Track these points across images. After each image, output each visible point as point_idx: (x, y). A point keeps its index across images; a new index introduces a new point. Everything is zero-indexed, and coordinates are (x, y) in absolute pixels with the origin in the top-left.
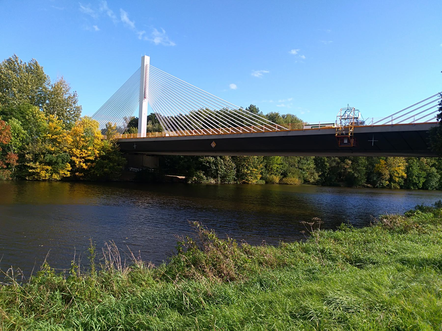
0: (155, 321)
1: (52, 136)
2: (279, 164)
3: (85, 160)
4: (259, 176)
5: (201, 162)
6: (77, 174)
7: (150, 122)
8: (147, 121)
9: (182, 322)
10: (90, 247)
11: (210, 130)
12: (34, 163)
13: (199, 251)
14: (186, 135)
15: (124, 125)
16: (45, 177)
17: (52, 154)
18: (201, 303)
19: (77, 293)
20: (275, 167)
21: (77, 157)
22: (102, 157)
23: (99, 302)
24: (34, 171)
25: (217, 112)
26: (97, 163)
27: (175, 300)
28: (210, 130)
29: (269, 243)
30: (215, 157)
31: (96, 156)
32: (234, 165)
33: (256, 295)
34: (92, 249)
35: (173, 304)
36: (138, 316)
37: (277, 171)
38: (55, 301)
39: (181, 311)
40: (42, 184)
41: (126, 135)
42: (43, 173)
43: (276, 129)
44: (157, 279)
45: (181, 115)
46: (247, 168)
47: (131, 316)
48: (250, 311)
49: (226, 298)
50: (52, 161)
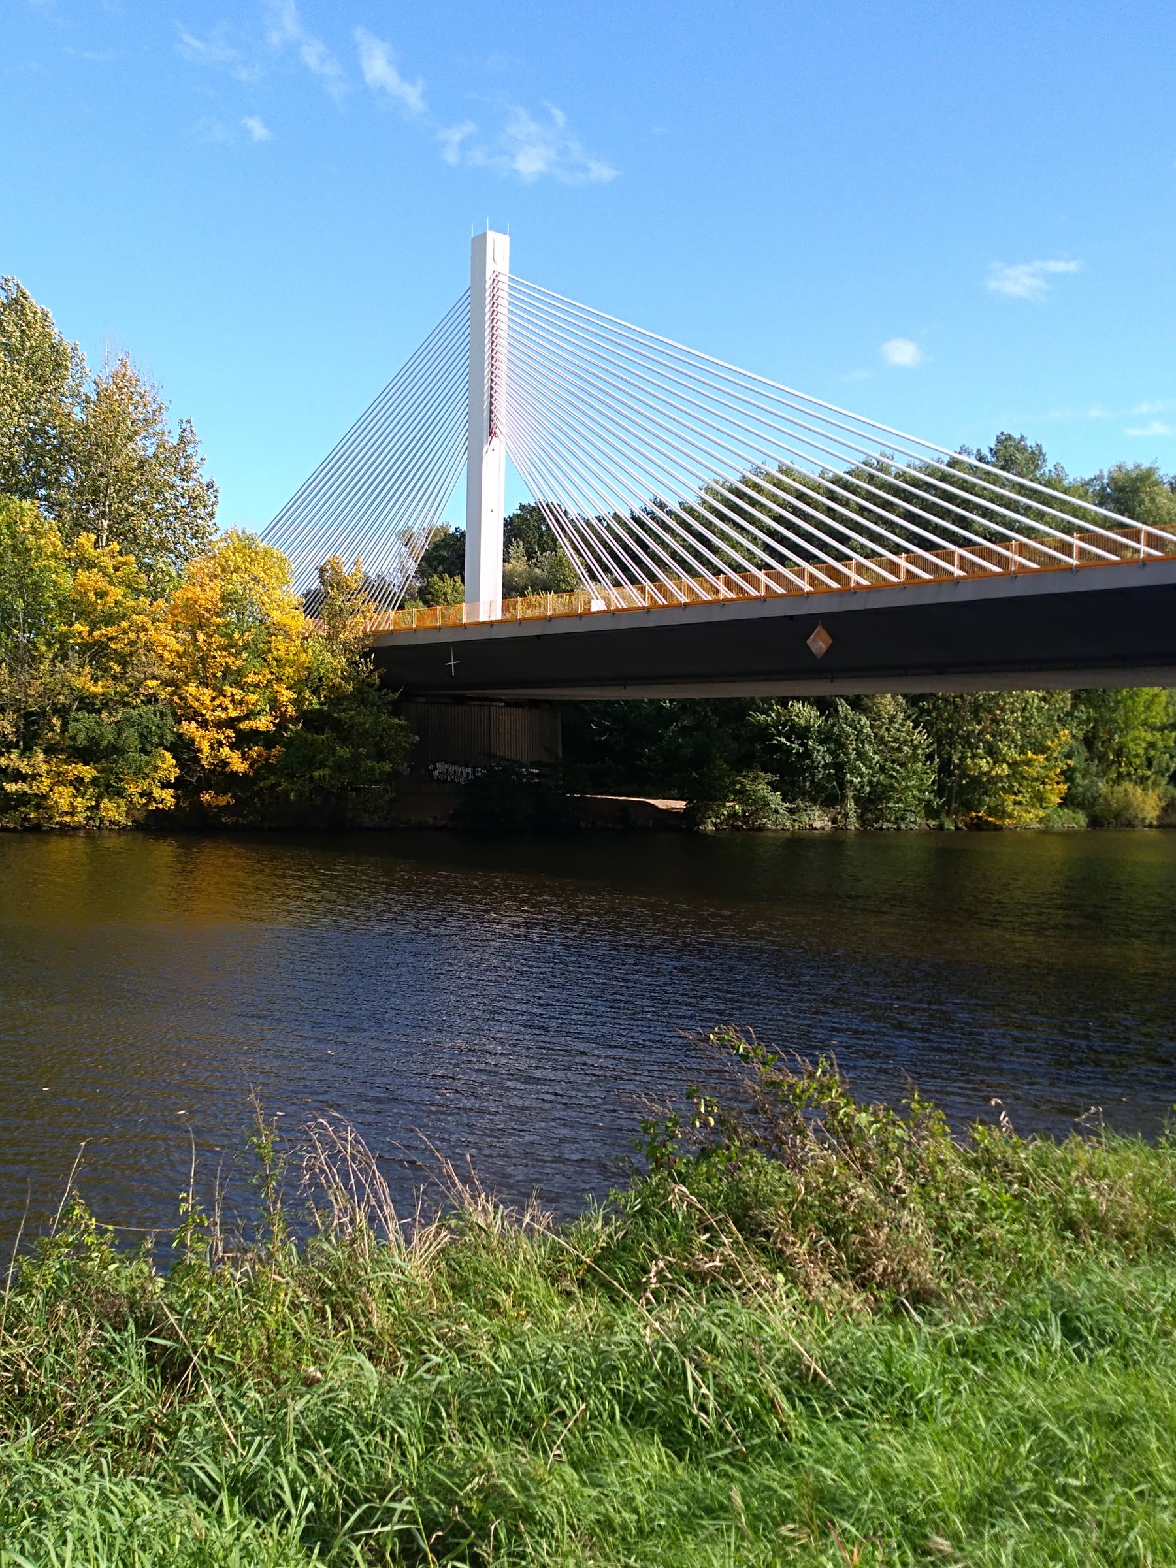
0: (557, 1483)
1: (90, 633)
2: (1162, 729)
3: (239, 732)
4: (1055, 793)
5: (763, 733)
6: (206, 797)
7: (518, 549)
8: (507, 544)
9: (682, 1495)
10: (258, 1134)
11: (800, 574)
12: (22, 754)
13: (759, 1158)
14: (684, 599)
15: (402, 569)
16: (72, 815)
17: (99, 712)
18: (774, 1408)
19: (210, 1338)
20: (1138, 740)
21: (204, 724)
22: (310, 719)
23: (310, 1382)
24: (26, 787)
25: (836, 481)
26: (289, 744)
27: (651, 1390)
28: (800, 574)
29: (1122, 1127)
30: (824, 705)
31: (283, 716)
32: (921, 737)
33: (1043, 1382)
34: (266, 1140)
35: (639, 1408)
36: (480, 1455)
37: (1149, 763)
38: (120, 1373)
39: (676, 1439)
40: (60, 849)
41: (414, 616)
42: (63, 797)
43: (1143, 548)
44: (566, 1284)
45: (662, 506)
46: (991, 751)
47: (449, 1453)
48: (1011, 1457)
49: (894, 1390)
50: (98, 744)
